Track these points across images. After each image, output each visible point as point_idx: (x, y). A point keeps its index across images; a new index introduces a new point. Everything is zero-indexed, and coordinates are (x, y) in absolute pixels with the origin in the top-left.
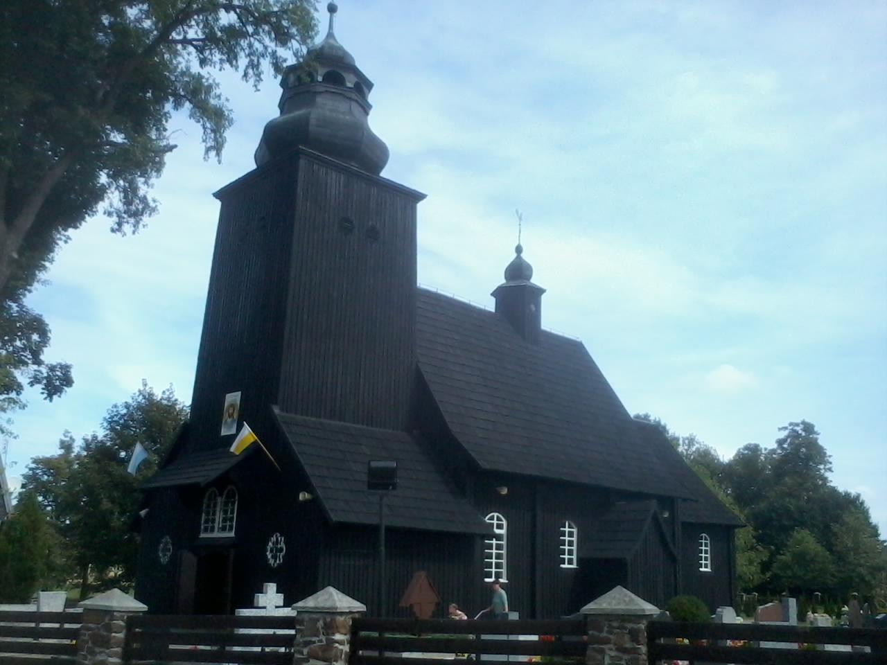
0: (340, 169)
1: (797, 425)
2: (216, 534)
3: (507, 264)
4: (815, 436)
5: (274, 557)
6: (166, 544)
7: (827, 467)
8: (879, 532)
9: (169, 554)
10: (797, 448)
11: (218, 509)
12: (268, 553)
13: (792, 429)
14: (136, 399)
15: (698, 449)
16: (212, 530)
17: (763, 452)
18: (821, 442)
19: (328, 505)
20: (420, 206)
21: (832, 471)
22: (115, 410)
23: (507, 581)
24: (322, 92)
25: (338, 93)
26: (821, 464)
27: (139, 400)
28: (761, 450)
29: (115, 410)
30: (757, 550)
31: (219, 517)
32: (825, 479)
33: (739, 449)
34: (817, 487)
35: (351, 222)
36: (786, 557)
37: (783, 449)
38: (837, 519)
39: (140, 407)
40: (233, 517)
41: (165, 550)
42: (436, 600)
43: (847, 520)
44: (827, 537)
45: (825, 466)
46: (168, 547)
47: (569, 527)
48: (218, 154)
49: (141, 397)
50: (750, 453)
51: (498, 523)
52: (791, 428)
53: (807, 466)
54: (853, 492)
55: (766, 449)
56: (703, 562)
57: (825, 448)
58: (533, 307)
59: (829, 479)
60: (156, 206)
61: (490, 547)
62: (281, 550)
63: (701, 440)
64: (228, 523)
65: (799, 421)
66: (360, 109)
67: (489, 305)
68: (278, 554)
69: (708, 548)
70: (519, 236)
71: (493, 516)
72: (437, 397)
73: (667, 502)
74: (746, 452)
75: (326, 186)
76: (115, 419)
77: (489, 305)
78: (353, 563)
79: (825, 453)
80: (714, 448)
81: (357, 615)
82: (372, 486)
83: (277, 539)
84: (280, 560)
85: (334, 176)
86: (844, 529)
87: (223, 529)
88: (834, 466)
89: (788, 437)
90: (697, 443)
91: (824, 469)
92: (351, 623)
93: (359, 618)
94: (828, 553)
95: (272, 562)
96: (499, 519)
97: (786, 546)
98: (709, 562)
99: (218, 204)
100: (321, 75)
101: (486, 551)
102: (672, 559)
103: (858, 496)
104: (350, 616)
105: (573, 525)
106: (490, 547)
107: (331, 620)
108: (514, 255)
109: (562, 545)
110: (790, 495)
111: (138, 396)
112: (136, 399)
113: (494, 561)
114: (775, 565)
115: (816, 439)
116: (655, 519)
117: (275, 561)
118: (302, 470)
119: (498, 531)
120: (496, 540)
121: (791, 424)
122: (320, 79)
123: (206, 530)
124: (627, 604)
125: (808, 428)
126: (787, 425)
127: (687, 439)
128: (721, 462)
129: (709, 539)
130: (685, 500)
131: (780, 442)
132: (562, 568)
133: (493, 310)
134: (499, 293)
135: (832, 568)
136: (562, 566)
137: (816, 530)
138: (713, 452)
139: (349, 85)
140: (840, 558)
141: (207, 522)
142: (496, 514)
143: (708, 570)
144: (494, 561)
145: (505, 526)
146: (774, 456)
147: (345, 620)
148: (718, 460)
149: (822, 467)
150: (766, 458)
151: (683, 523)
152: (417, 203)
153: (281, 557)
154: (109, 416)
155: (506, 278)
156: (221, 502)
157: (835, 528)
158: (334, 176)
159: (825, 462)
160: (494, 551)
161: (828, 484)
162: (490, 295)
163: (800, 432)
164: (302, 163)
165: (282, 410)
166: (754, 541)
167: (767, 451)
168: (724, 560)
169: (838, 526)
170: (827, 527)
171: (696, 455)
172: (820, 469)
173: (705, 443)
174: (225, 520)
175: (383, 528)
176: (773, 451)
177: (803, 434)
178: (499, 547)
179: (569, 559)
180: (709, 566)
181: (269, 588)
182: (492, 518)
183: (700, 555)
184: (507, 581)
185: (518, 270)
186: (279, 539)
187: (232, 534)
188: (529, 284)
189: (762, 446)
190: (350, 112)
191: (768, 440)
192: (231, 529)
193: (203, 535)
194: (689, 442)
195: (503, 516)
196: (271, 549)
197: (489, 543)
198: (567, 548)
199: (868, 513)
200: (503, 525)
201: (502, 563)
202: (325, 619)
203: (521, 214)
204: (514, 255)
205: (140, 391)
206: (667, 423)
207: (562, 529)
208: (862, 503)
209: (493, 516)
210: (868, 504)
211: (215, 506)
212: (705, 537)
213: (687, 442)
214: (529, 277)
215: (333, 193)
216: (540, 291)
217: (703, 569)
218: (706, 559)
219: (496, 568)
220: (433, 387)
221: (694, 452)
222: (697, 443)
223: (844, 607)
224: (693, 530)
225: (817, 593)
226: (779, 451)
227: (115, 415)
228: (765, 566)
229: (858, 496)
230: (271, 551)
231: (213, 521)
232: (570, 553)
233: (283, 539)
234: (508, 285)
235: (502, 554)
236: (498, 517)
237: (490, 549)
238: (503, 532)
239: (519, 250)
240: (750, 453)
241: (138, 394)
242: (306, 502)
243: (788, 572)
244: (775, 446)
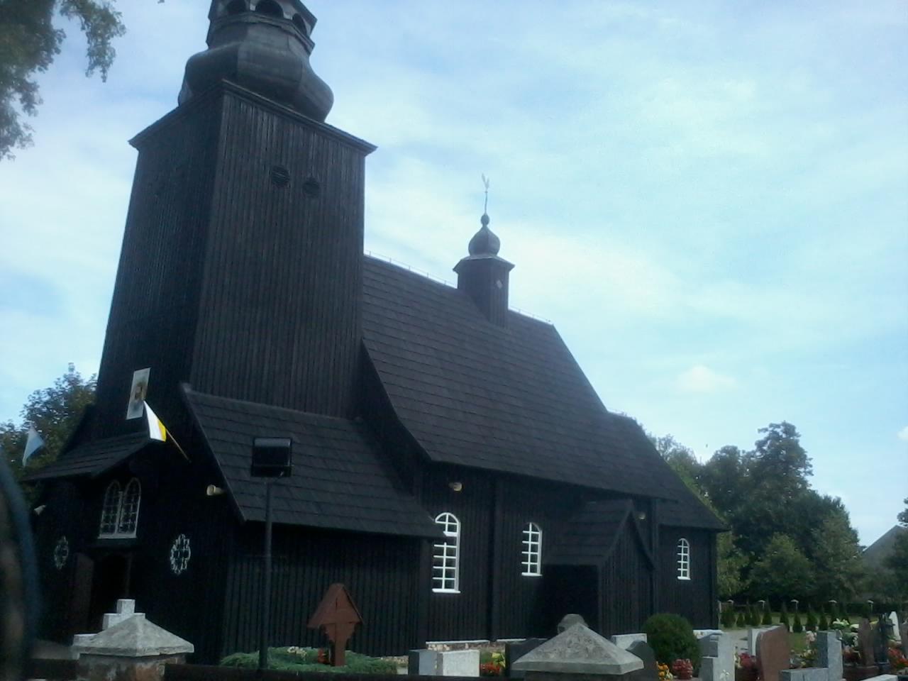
0: (272, 110)
1: (778, 426)
2: (117, 535)
4: (796, 438)
5: (178, 563)
6: (63, 545)
7: (807, 470)
8: (858, 538)
9: (65, 558)
10: (776, 451)
11: (119, 506)
12: (171, 558)
13: (772, 431)
14: (60, 386)
15: (675, 451)
16: (112, 530)
17: (741, 454)
18: (802, 444)
19: (239, 501)
20: (369, 160)
21: (813, 475)
22: (37, 396)
23: (459, 592)
24: (254, 23)
25: (273, 26)
26: (801, 467)
27: (64, 386)
28: (739, 453)
29: (37, 396)
30: (737, 556)
31: (120, 514)
32: (804, 483)
33: (717, 451)
34: (796, 492)
35: (285, 172)
36: (764, 564)
37: (762, 451)
38: (816, 524)
39: (65, 395)
40: (135, 515)
41: (61, 553)
42: (356, 619)
43: (827, 525)
44: (806, 541)
45: (805, 469)
46: (65, 549)
47: (533, 530)
48: (104, 71)
49: (66, 383)
50: (728, 456)
51: (451, 526)
52: (771, 429)
53: (786, 469)
54: (833, 495)
55: (744, 452)
56: (682, 570)
57: (806, 450)
58: (499, 284)
59: (809, 483)
60: (30, 134)
61: (440, 552)
62: (186, 554)
63: (678, 441)
64: (130, 522)
65: (779, 422)
66: (298, 43)
67: (451, 280)
68: (183, 559)
69: (687, 555)
70: (486, 205)
71: (445, 517)
72: (383, 378)
73: (644, 502)
74: (724, 454)
75: (256, 127)
76: (37, 406)
77: (451, 280)
78: (257, 570)
79: (806, 456)
80: (691, 450)
81: (176, 660)
82: (257, 471)
83: (182, 541)
84: (184, 567)
85: (265, 118)
86: (824, 534)
87: (124, 529)
88: (815, 470)
89: (768, 439)
90: (674, 444)
91: (804, 472)
92: (163, 673)
93: (178, 666)
94: (807, 559)
95: (175, 568)
96: (451, 520)
97: (763, 551)
98: (688, 570)
99: (134, 154)
100: (254, 5)
101: (435, 556)
102: (648, 566)
103: (838, 501)
104: (164, 661)
105: (537, 526)
106: (440, 552)
107: (128, 669)
108: (480, 226)
110: (769, 498)
111: (63, 382)
112: (60, 386)
113: (444, 568)
114: (752, 571)
115: (797, 441)
116: (631, 523)
117: (179, 567)
118: (212, 460)
119: (447, 533)
120: (447, 544)
121: (771, 425)
122: (253, 8)
123: (106, 530)
124: (590, 657)
125: (789, 430)
126: (767, 426)
127: (664, 439)
128: (698, 465)
129: (688, 544)
130: (664, 500)
131: (760, 445)
133: (455, 286)
134: (463, 268)
135: (811, 575)
136: (524, 574)
137: (795, 535)
138: (690, 454)
139: (287, 16)
140: (820, 565)
141: (107, 520)
142: (448, 514)
143: (687, 578)
144: (444, 568)
145: (458, 529)
146: (752, 459)
147: (154, 667)
148: (696, 461)
149: (802, 470)
150: (744, 461)
151: (661, 526)
152: (365, 156)
153: (185, 562)
154: (30, 403)
155: (470, 251)
156: (123, 497)
157: (816, 533)
158: (265, 118)
159: (805, 466)
160: (445, 557)
161: (808, 488)
162: (452, 270)
163: (781, 434)
164: (227, 100)
165: (194, 389)
166: (734, 546)
167: (745, 454)
168: (704, 568)
169: (818, 530)
170: (808, 533)
171: (673, 457)
172: (800, 472)
173: (682, 445)
174: (126, 519)
175: (270, 528)
176: (750, 455)
177: (784, 436)
178: (451, 552)
179: (531, 566)
180: (688, 574)
181: (124, 606)
182: (443, 519)
183: (679, 562)
184: (459, 592)
185: (484, 243)
186: (185, 540)
187: (133, 535)
188: (496, 258)
189: (740, 448)
190: (288, 48)
191: (747, 442)
192: (132, 529)
193: (102, 536)
194: (666, 444)
195: (457, 517)
196: (175, 552)
197: (529, 527)
198: (530, 553)
199: (847, 518)
200: (456, 526)
201: (454, 570)
202: (119, 667)
203: (488, 181)
204: (478, 227)
205: (65, 376)
206: (643, 423)
207: (524, 532)
208: (842, 507)
210: (848, 508)
211: (117, 500)
212: (684, 542)
213: (663, 442)
214: (496, 251)
215: (264, 136)
216: (508, 267)
218: (685, 566)
219: (446, 577)
220: (378, 367)
221: (671, 453)
222: (674, 444)
223: (836, 620)
224: (672, 534)
225: (795, 601)
226: (758, 454)
227: (37, 402)
228: (744, 572)
229: (838, 501)
230: (176, 556)
231: (113, 521)
232: (534, 559)
233: (188, 542)
234: (472, 258)
235: (455, 559)
236: (450, 517)
237: (440, 555)
238: (456, 534)
239: (485, 220)
240: (728, 456)
241: (62, 379)
242: (215, 497)
243: (766, 579)
244: (755, 448)
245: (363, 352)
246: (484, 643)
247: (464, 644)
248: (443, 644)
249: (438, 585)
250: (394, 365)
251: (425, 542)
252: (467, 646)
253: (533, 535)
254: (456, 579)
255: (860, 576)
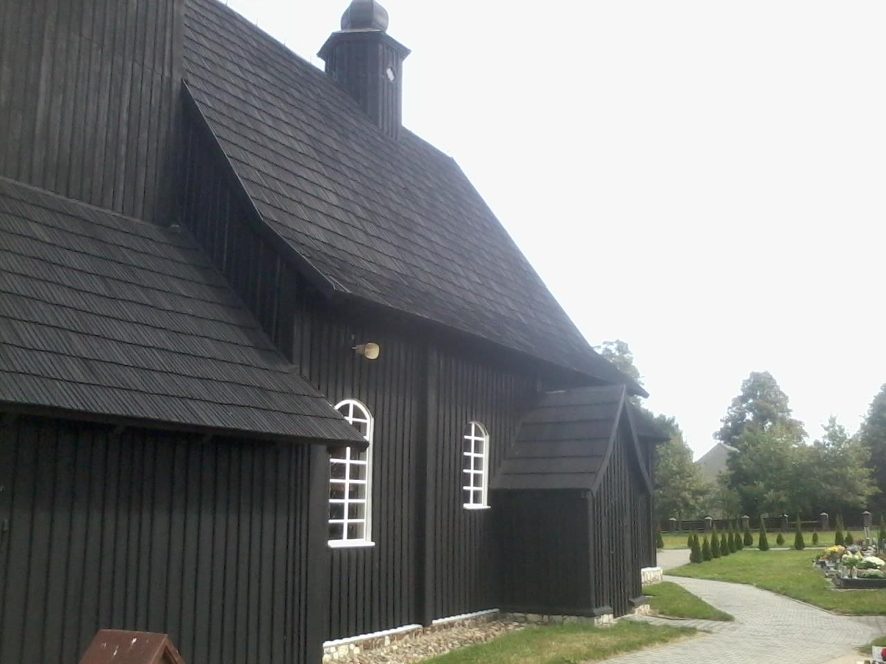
1: (611, 344)
3: (342, 13)
23: (373, 544)
61: (339, 471)
71: (347, 406)
96: (358, 413)
106: (339, 471)
109: (466, 468)
121: (605, 343)
132: (332, 550)
134: (333, 49)
142: (352, 403)
163: (614, 351)
177: (617, 354)
184: (373, 544)
195: (368, 407)
197: (336, 464)
198: (347, 481)
209: (347, 406)
217: (470, 506)
236: (355, 408)
245: (184, 94)
246: (413, 631)
247: (383, 637)
248: (349, 644)
249: (336, 532)
250: (246, 137)
251: (322, 448)
252: (387, 642)
253: (352, 466)
254: (366, 521)
255: (702, 493)
